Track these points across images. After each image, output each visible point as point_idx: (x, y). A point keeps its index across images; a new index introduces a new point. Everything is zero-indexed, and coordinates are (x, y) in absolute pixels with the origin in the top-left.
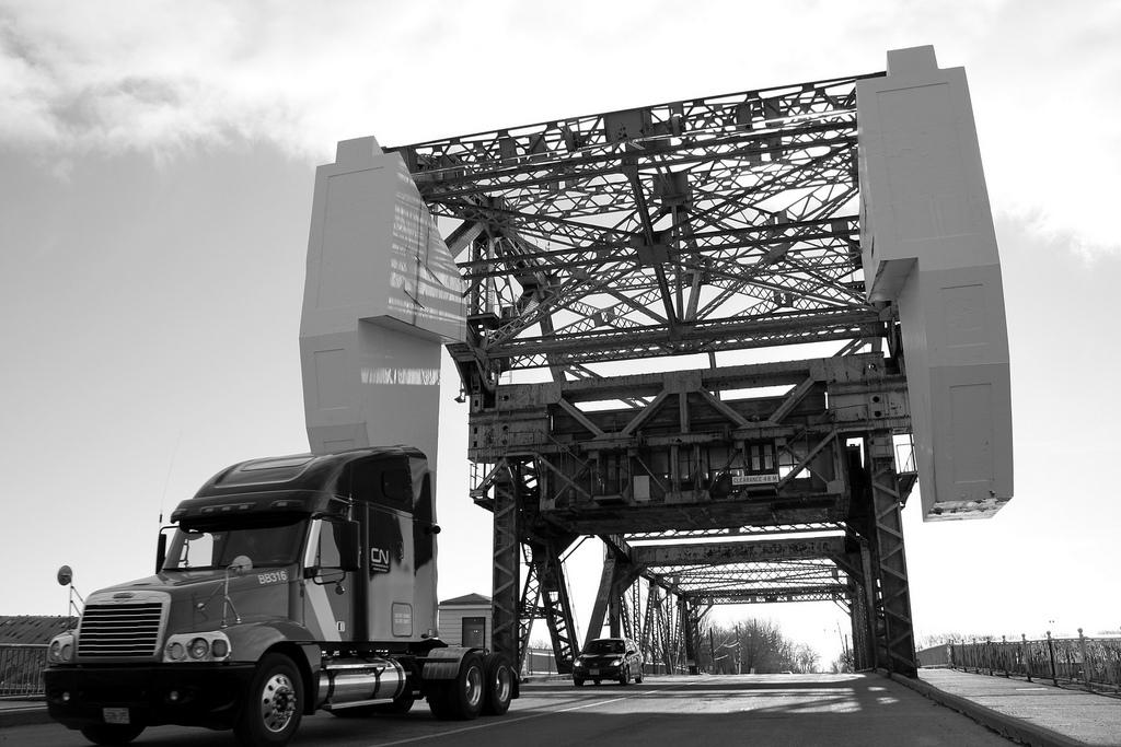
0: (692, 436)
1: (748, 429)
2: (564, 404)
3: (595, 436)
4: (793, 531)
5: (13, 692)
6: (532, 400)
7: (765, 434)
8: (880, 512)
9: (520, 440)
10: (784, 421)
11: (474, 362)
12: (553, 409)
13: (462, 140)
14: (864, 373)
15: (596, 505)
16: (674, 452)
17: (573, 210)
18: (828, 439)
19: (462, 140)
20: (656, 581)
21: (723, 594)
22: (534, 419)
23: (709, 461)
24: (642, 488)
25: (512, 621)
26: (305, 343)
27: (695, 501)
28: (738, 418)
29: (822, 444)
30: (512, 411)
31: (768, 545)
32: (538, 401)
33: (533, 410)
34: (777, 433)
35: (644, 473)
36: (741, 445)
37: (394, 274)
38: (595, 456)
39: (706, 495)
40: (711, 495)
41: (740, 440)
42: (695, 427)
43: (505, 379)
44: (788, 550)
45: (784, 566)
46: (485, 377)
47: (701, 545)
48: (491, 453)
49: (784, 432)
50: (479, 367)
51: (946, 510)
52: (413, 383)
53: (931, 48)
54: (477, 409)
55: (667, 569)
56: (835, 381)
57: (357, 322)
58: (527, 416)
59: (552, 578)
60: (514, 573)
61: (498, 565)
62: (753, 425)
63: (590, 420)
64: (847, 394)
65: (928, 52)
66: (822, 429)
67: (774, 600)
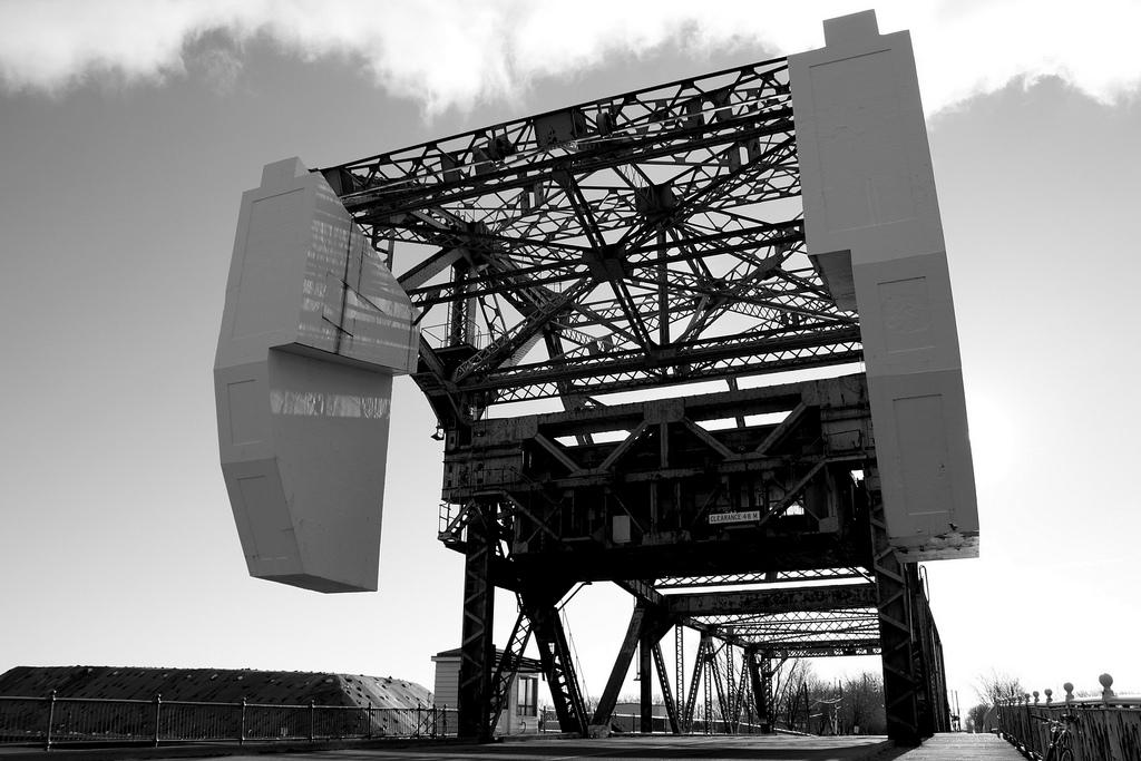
0: (673, 471)
2: (540, 439)
5: (17, 739)
6: (508, 435)
7: (751, 466)
8: (878, 552)
9: (495, 478)
10: (771, 453)
12: (530, 445)
15: (569, 548)
16: (653, 490)
17: (558, 232)
19: (393, 158)
20: (708, 632)
21: (793, 646)
22: (510, 456)
25: (480, 674)
26: (219, 374)
28: (723, 450)
31: (826, 592)
32: (514, 438)
33: (507, 445)
34: (765, 465)
35: (622, 513)
36: (724, 480)
37: (308, 301)
39: (687, 536)
41: (724, 474)
43: (494, 412)
45: (838, 615)
46: (460, 412)
49: (771, 464)
52: (349, 415)
53: (873, 11)
54: (452, 446)
55: (723, 619)
56: (829, 405)
58: (503, 452)
59: (548, 628)
60: (484, 622)
61: (468, 614)
62: (739, 456)
64: (842, 420)
65: (869, 17)
67: (853, 653)
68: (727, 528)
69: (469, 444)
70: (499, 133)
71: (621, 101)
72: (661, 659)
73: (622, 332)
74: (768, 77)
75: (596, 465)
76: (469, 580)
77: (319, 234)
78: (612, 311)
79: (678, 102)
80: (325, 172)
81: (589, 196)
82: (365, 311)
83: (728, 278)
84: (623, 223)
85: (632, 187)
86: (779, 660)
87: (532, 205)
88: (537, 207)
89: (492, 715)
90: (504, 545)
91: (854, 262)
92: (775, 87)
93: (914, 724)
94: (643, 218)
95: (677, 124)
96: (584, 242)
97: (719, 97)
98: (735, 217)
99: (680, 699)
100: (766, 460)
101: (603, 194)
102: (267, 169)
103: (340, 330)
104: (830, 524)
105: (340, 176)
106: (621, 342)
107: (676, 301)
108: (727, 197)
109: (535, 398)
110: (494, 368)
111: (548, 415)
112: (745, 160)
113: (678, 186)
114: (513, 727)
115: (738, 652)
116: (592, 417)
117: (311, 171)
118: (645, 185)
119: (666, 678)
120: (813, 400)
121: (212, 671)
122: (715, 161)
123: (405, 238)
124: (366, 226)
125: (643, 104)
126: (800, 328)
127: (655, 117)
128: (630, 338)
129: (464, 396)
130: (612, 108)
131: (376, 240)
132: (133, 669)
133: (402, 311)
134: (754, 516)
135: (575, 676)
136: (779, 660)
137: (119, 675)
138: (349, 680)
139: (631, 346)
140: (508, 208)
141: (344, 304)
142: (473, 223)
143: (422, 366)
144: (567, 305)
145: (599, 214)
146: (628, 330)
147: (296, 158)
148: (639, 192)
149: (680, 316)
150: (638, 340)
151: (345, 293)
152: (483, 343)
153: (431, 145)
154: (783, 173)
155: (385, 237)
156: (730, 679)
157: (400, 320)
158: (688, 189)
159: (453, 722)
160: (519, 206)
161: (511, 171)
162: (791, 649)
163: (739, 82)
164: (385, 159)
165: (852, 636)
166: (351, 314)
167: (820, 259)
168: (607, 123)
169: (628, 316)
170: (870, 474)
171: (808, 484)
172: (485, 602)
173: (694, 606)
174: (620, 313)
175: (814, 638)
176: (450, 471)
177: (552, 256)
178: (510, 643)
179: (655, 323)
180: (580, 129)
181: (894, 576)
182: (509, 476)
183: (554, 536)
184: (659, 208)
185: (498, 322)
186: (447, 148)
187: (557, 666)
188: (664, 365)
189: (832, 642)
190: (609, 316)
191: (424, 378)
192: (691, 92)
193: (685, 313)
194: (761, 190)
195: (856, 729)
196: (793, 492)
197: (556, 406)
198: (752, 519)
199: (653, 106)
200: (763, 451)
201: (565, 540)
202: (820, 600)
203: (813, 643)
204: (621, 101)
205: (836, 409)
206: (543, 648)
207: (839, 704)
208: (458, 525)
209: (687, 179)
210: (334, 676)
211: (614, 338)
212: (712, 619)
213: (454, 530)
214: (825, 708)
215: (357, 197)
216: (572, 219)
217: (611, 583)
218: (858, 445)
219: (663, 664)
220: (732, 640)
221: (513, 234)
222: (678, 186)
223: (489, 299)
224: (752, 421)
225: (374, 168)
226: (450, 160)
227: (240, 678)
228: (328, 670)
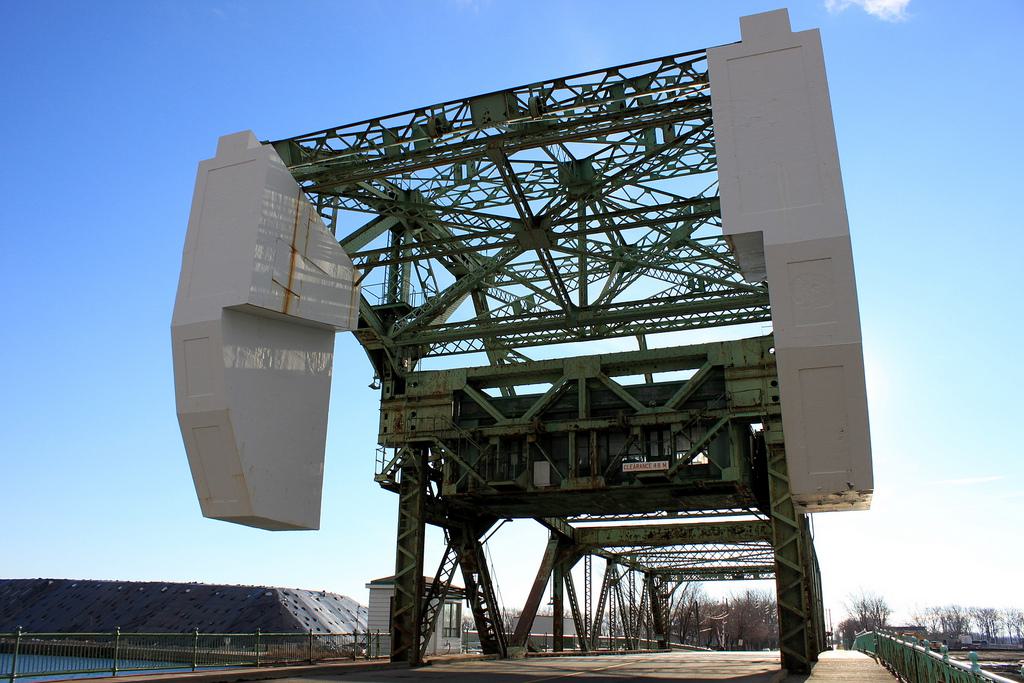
1: (645, 415)
2: (469, 390)
3: (497, 422)
4: (730, 515)
6: (439, 386)
7: (661, 420)
8: (775, 499)
9: (427, 425)
11: (383, 350)
12: (459, 395)
13: (338, 132)
14: (762, 357)
15: (494, 491)
16: (572, 437)
17: (487, 200)
18: (720, 425)
19: (338, 132)
20: (612, 560)
23: (608, 446)
24: (542, 473)
25: (412, 604)
27: (591, 487)
28: (635, 403)
29: (713, 430)
30: (420, 398)
33: (440, 396)
34: (673, 418)
36: (637, 431)
38: (495, 441)
39: (601, 481)
40: (608, 482)
41: (636, 426)
42: (594, 413)
43: (426, 364)
44: (725, 533)
45: (741, 547)
47: (642, 527)
48: (400, 439)
50: (389, 355)
51: (812, 502)
54: (388, 395)
55: (628, 549)
56: (732, 365)
57: (221, 310)
58: (434, 402)
59: (473, 560)
62: (649, 410)
63: (495, 407)
64: (745, 378)
65: (782, 15)
66: (718, 414)
67: (741, 578)
68: (638, 476)
69: (404, 393)
70: (437, 112)
71: (551, 85)
72: (572, 585)
73: (543, 292)
74: (686, 66)
75: (519, 416)
76: (402, 518)
77: (270, 201)
78: (534, 272)
79: (604, 86)
80: (274, 144)
81: (517, 168)
82: (311, 274)
83: (640, 244)
84: (547, 194)
85: (556, 161)
86: (674, 584)
87: (465, 176)
88: (469, 177)
89: (422, 640)
90: (434, 484)
91: (767, 242)
92: (692, 76)
93: (804, 656)
94: (564, 189)
95: (601, 107)
96: (511, 211)
97: (642, 83)
98: (648, 190)
99: (588, 613)
100: (675, 413)
101: (529, 167)
102: (223, 140)
103: (288, 291)
104: (733, 473)
105: (290, 149)
106: (542, 301)
107: (592, 264)
108: (624, 167)
109: (464, 352)
110: (425, 326)
111: (476, 369)
112: (660, 140)
113: (598, 161)
114: (439, 646)
115: (639, 577)
116: (516, 371)
117: (263, 143)
118: (568, 159)
119: (576, 602)
120: (716, 360)
121: (162, 584)
122: (632, 140)
123: (349, 207)
124: (313, 195)
125: (570, 88)
126: (707, 294)
127: (579, 100)
128: (549, 297)
129: (400, 349)
130: (542, 92)
131: (320, 206)
132: (90, 582)
133: (344, 272)
134: (663, 465)
135: (496, 603)
136: (674, 584)
137: (77, 587)
138: (286, 594)
139: (552, 306)
140: (443, 179)
141: (292, 268)
142: (409, 191)
143: (362, 323)
144: (499, 267)
145: (525, 185)
146: (549, 291)
147: (249, 131)
148: (562, 166)
149: (596, 278)
150: (559, 301)
151: (293, 257)
152: (418, 301)
153: (375, 122)
154: (694, 151)
155: (328, 205)
156: (632, 599)
157: (343, 282)
158: (607, 165)
159: (387, 645)
160: (452, 177)
161: (448, 147)
162: (686, 574)
163: (661, 70)
164: (331, 133)
165: (742, 564)
166: (298, 276)
167: (733, 238)
168: (539, 106)
169: (549, 276)
170: (768, 429)
171: (713, 437)
172: (416, 538)
173: (602, 539)
174: (541, 274)
175: (707, 565)
176: (386, 418)
177: (483, 226)
178: (439, 574)
179: (573, 284)
180: (512, 110)
181: (788, 521)
182: (440, 424)
183: (481, 480)
184: (580, 182)
185: (430, 281)
186: (388, 124)
187: (480, 594)
188: (582, 324)
189: (723, 568)
190: (530, 276)
191: (363, 332)
192: (617, 78)
193: (600, 275)
194: (673, 167)
195: (741, 642)
196: (699, 445)
197: (482, 360)
198: (662, 468)
199: (579, 91)
200: (672, 405)
201: (489, 484)
202: (716, 535)
203: (705, 569)
204: (551, 85)
205: (740, 369)
206: (468, 578)
207: (726, 619)
208: (392, 468)
209: (607, 154)
210: (273, 590)
211: (536, 299)
212: (618, 550)
213: (389, 473)
214: (713, 624)
215: (308, 167)
216: (500, 189)
217: (532, 520)
218: (758, 402)
219: (573, 589)
220: (634, 566)
221: (445, 202)
222: (598, 161)
223: (423, 262)
224: (659, 378)
225: (321, 141)
226: (390, 134)
227: (188, 591)
228: (268, 584)
